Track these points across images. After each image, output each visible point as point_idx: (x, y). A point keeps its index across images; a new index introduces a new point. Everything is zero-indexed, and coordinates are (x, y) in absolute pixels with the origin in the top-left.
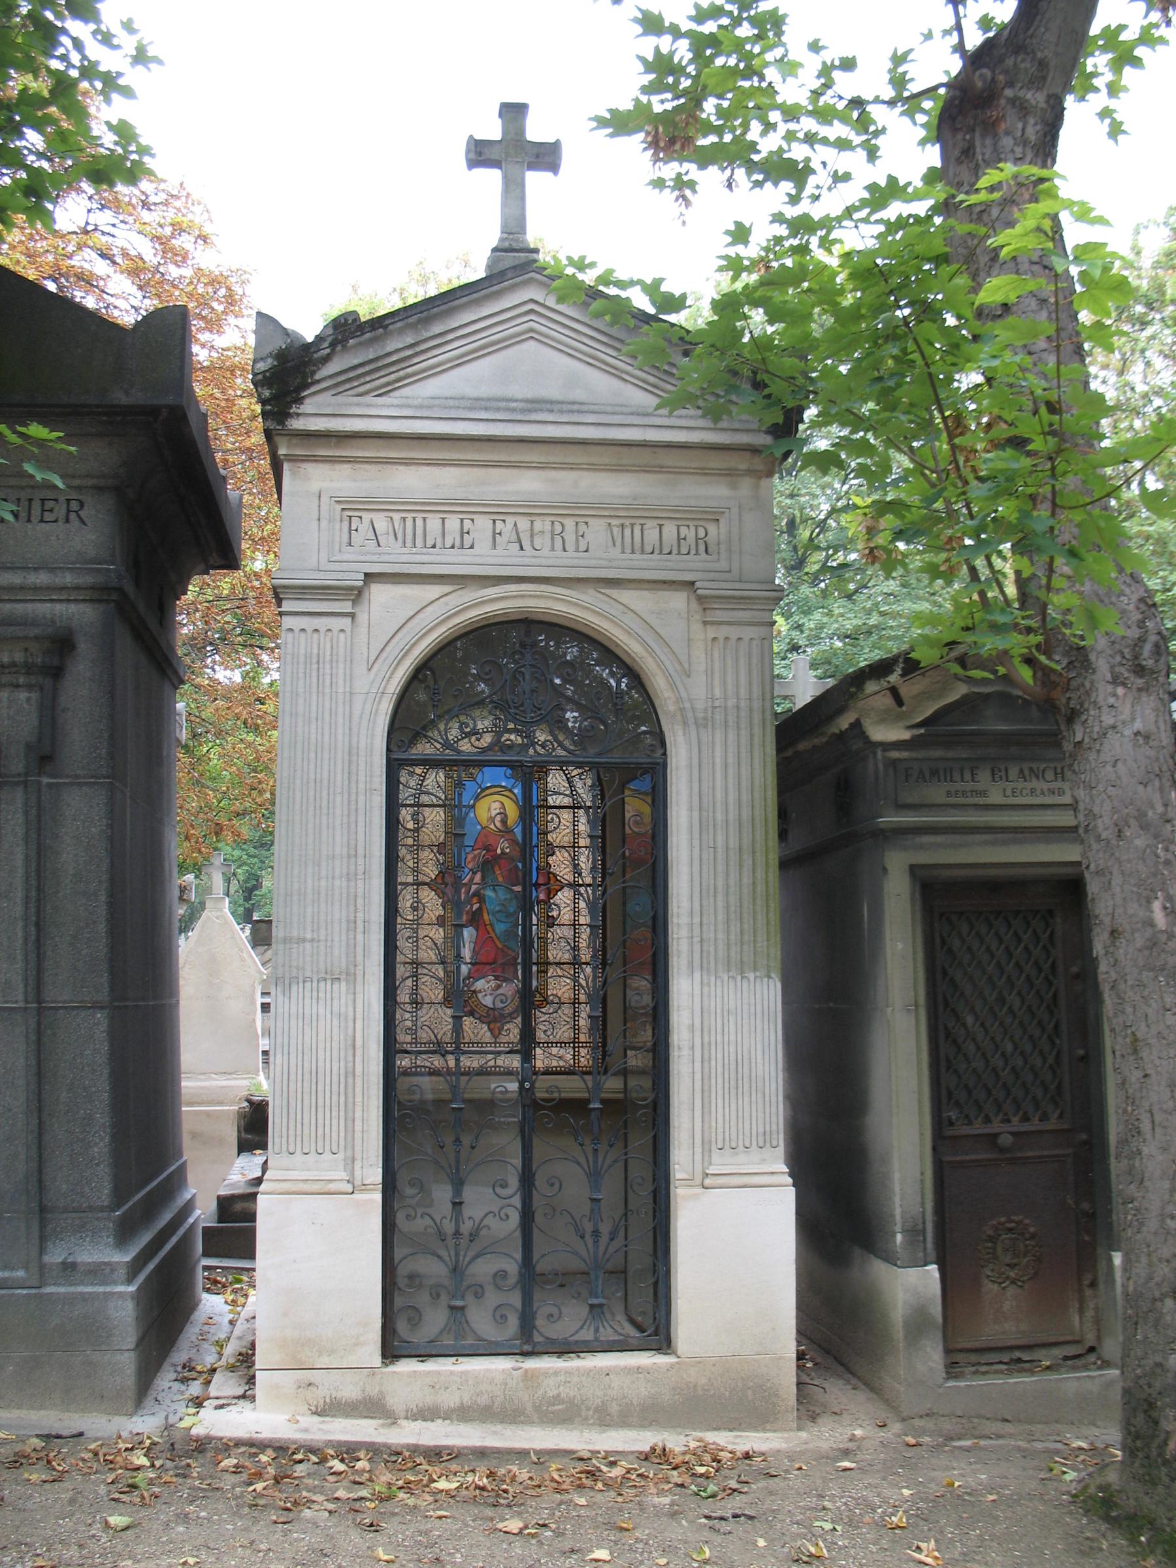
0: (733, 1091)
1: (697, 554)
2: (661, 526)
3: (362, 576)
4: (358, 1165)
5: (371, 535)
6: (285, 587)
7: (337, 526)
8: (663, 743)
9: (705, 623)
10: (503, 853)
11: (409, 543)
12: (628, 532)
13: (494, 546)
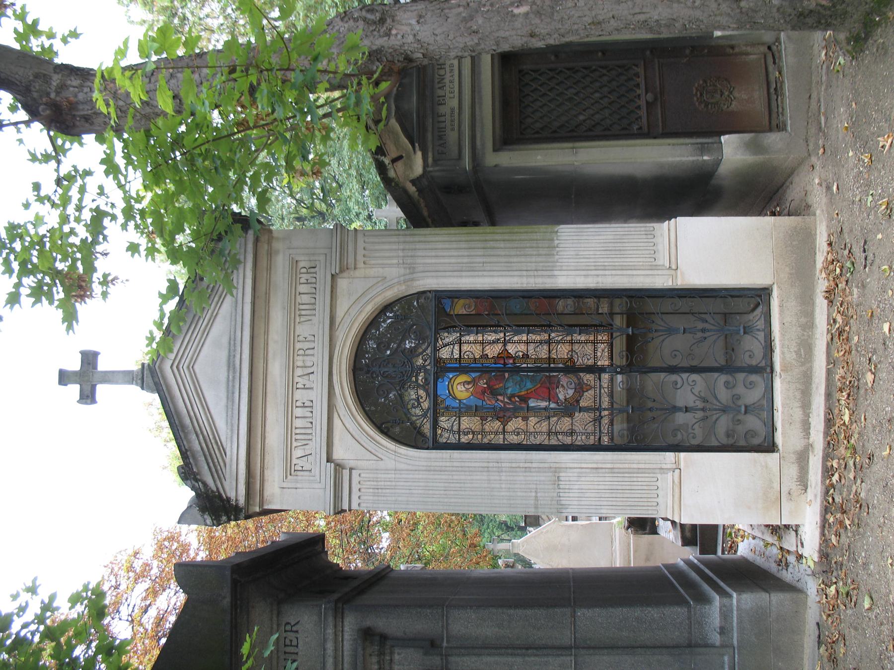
1: (316, 273)
3: (329, 464)
4: (664, 466)
5: (305, 459)
6: (335, 508)
7: (300, 478)
8: (424, 292)
11: (310, 437)
12: (303, 312)
13: (312, 388)
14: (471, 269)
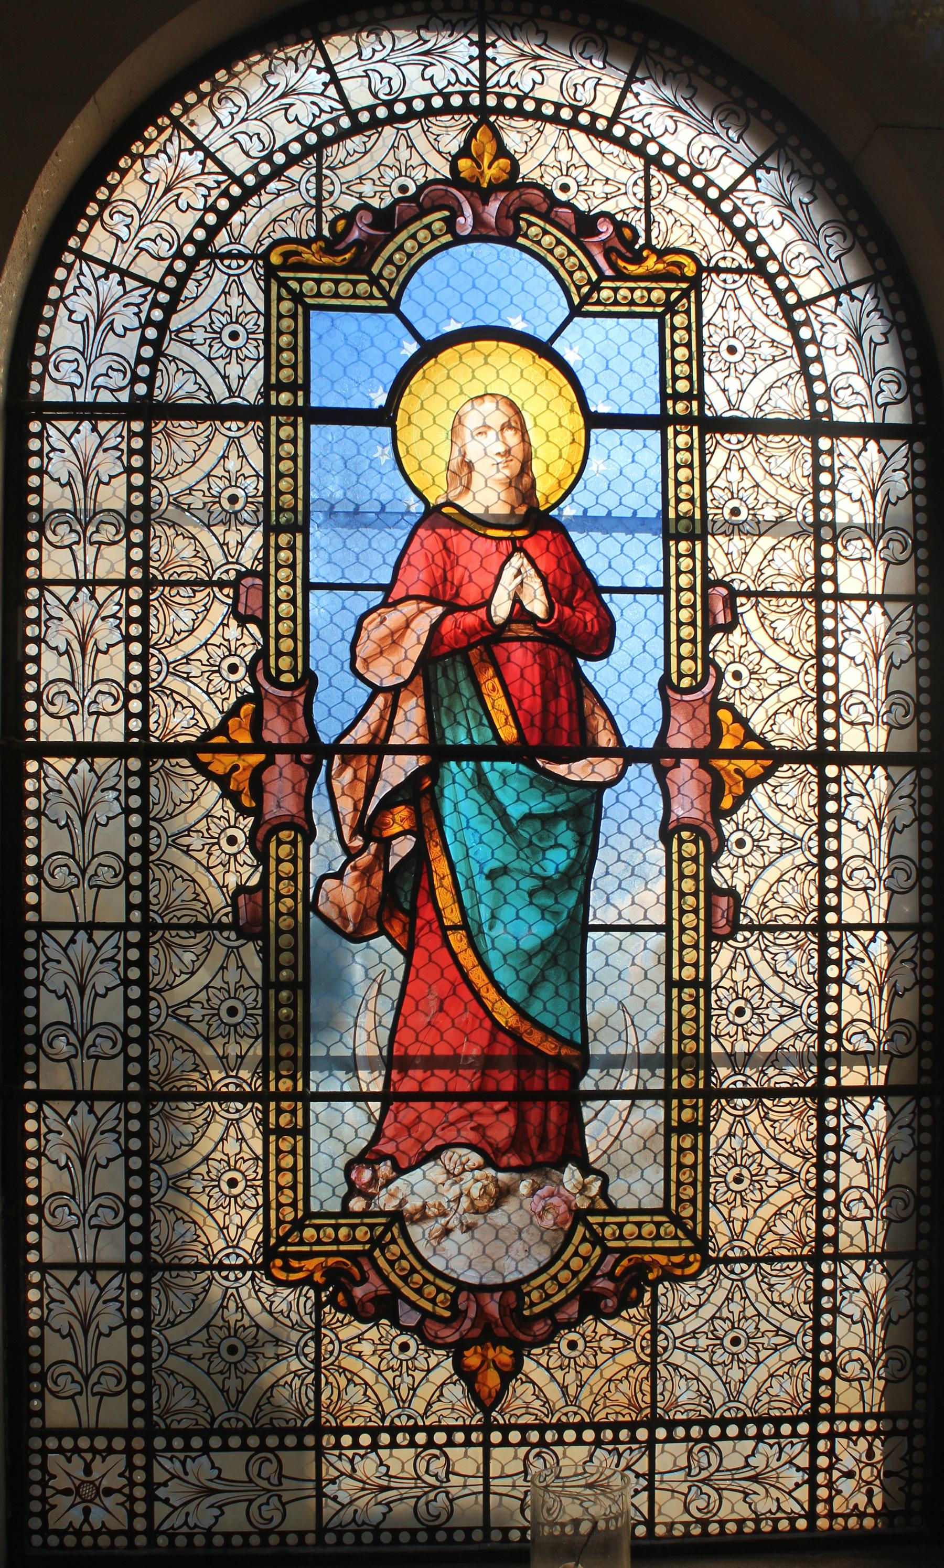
10: (519, 613)
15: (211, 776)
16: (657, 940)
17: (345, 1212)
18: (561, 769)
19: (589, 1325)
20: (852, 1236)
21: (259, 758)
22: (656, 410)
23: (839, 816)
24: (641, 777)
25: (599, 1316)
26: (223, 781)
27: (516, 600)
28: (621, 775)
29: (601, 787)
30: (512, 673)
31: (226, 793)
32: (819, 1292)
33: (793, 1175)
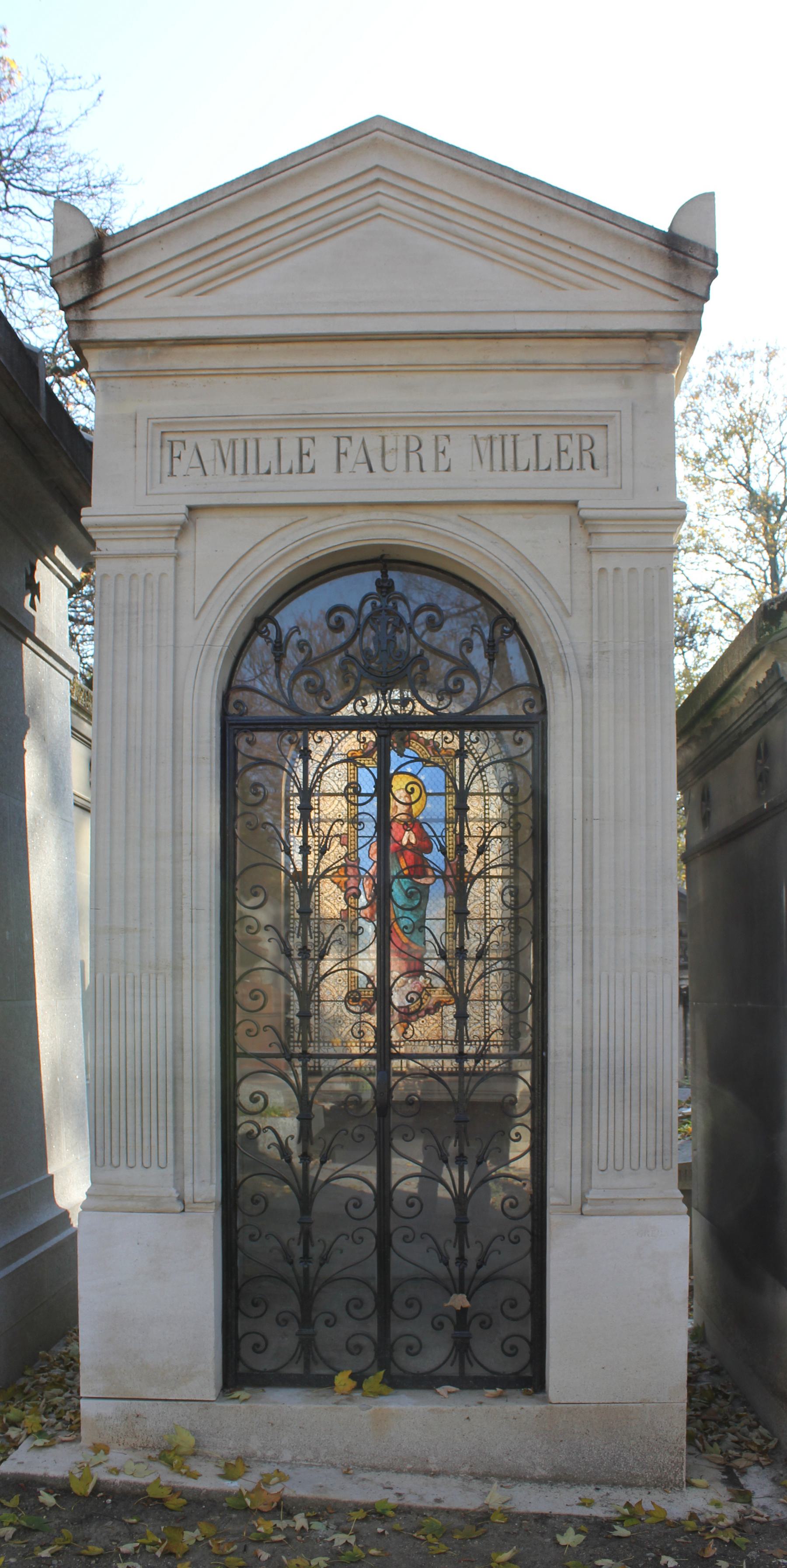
0: (619, 1105)
1: (581, 467)
2: (537, 436)
3: (184, 510)
4: (188, 1181)
5: (196, 462)
6: (97, 526)
7: (157, 452)
8: (544, 700)
9: (590, 551)
10: (409, 843)
11: (240, 469)
12: (497, 445)
13: (339, 469)
14: (63, 975)
15: (335, 883)
16: (444, 921)
17: (367, 988)
18: (419, 881)
19: (427, 1017)
20: (493, 995)
21: (346, 879)
22: (443, 791)
23: (489, 891)
24: (440, 882)
25: (430, 1014)
26: (338, 884)
27: (409, 840)
28: (434, 882)
29: (429, 885)
30: (407, 857)
31: (338, 887)
32: (485, 1010)
33: (326, 898)
